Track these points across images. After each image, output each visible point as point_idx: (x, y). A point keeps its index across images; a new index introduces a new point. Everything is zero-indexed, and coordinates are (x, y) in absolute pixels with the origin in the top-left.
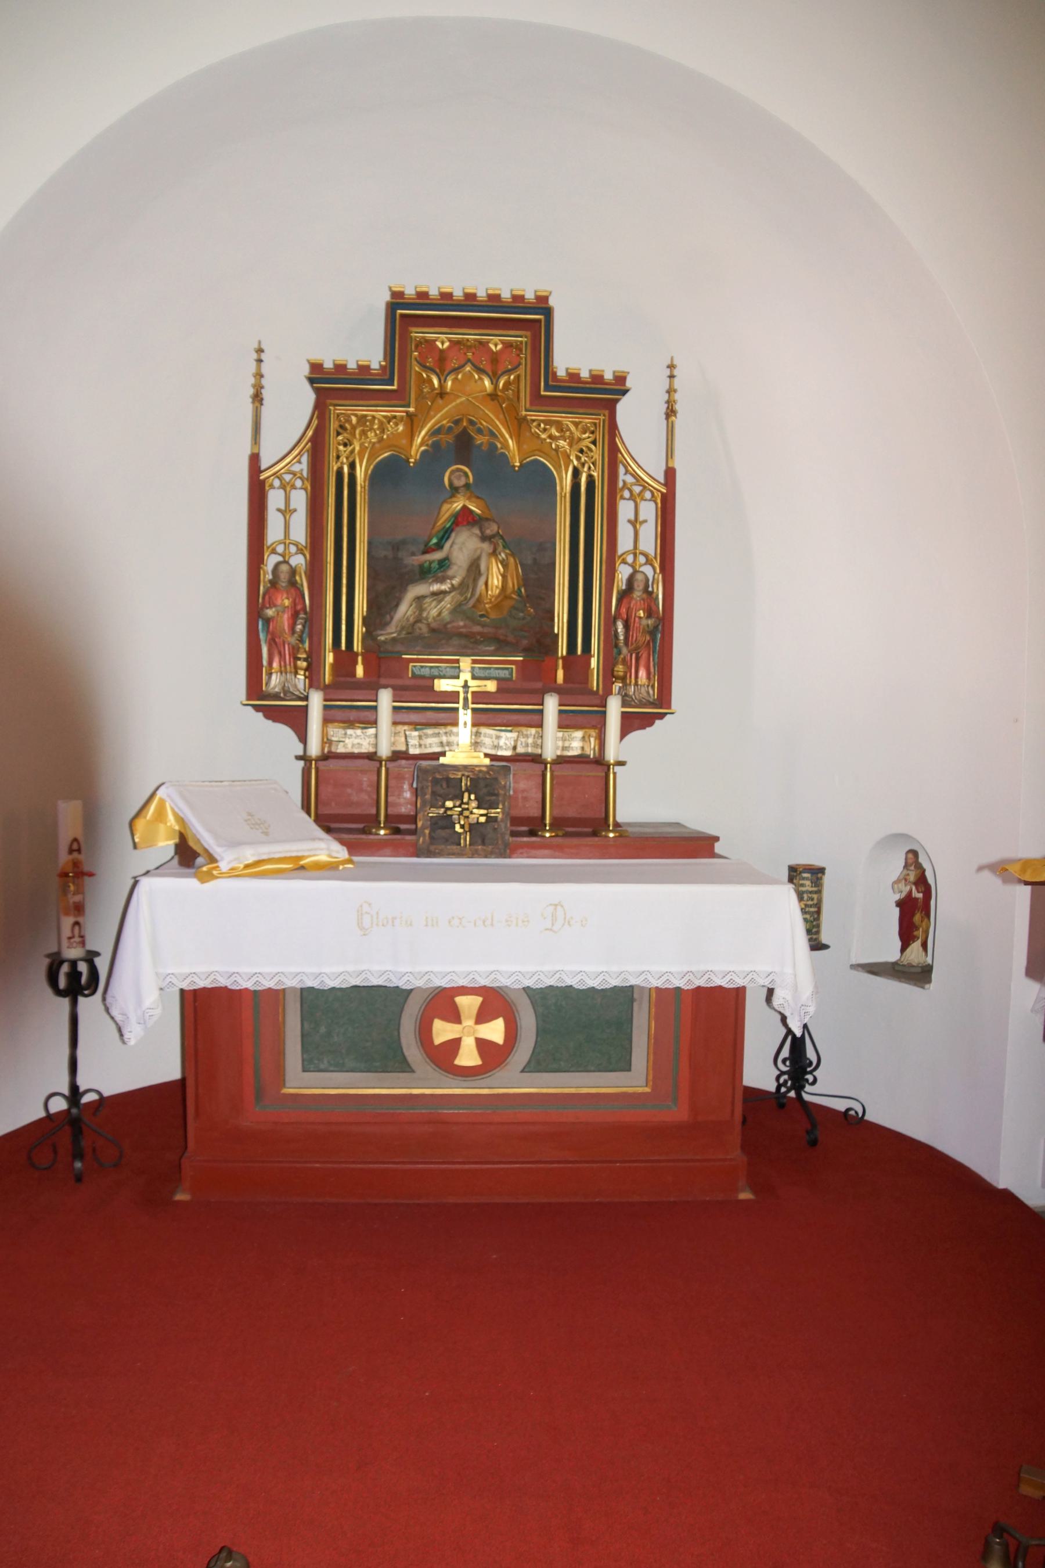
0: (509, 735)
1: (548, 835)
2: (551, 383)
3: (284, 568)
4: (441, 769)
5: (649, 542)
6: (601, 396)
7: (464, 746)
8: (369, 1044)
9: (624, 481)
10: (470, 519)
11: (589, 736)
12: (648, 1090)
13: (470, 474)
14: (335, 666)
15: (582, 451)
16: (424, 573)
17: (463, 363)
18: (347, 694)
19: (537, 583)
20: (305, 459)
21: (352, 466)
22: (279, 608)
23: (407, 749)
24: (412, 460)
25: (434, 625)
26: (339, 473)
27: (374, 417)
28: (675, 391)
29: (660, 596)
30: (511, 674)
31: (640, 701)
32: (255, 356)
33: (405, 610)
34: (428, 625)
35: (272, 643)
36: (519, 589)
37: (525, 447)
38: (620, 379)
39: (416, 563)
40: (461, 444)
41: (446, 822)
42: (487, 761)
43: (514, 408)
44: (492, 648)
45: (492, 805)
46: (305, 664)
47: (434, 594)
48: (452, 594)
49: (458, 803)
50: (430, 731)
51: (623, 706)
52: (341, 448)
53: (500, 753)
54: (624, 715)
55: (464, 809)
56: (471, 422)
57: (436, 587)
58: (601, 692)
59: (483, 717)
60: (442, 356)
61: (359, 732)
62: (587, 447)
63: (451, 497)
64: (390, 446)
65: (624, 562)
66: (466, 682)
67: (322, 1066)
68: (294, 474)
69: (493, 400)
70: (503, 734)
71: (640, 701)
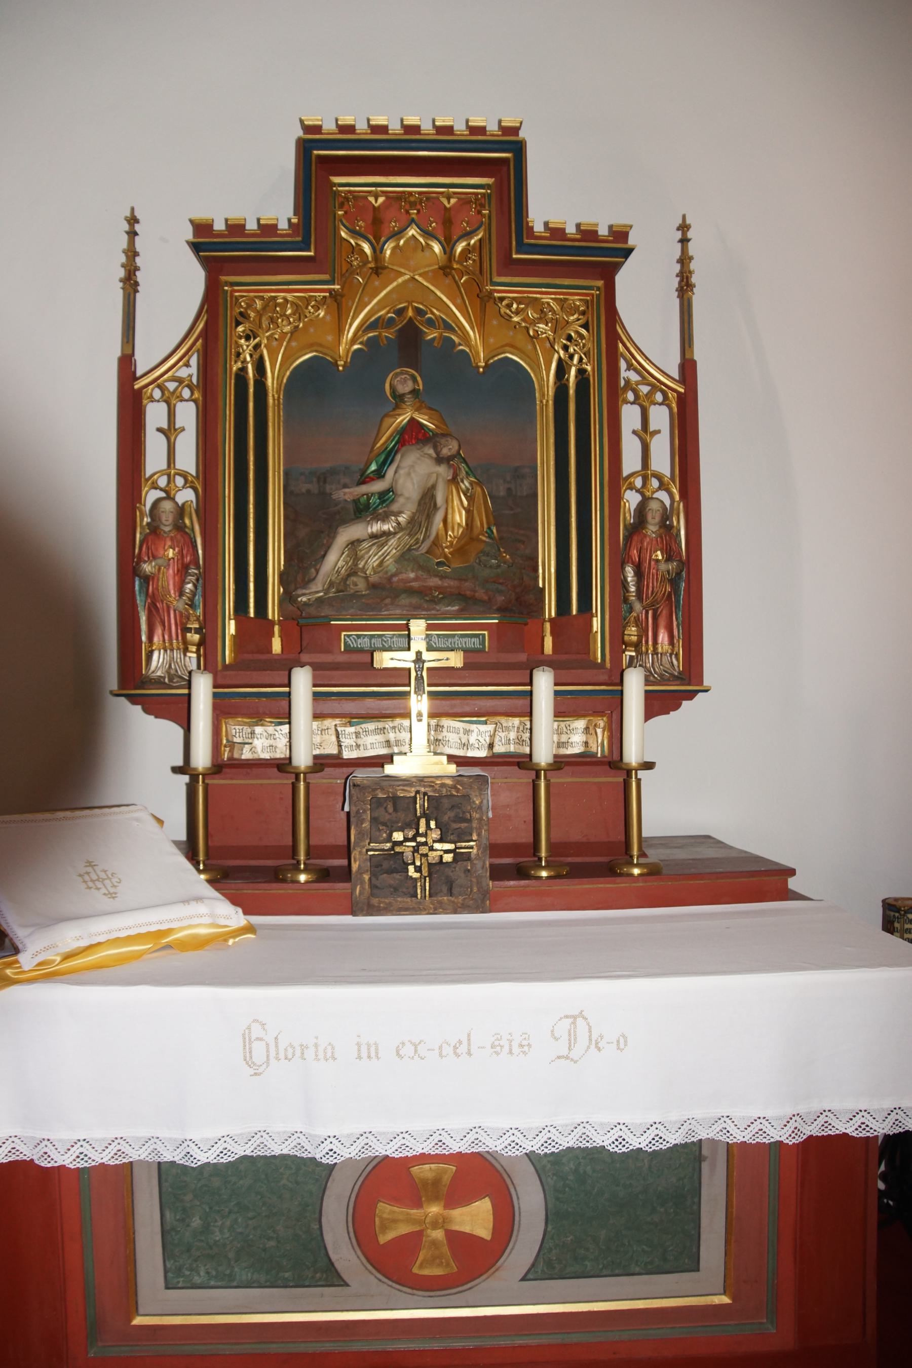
0: (483, 728)
1: (544, 874)
2: (526, 241)
3: (167, 506)
4: (384, 784)
5: (662, 460)
6: (597, 257)
7: (419, 749)
8: (273, 1243)
10: (420, 436)
12: (725, 1300)
13: (419, 379)
14: (238, 639)
15: (569, 338)
16: (362, 510)
18: (256, 677)
19: (511, 517)
20: (194, 361)
22: (160, 561)
23: (340, 752)
25: (374, 579)
27: (285, 299)
28: (691, 258)
29: (683, 532)
31: (661, 675)
32: (126, 227)
33: (334, 560)
34: (366, 578)
35: (153, 611)
36: (489, 528)
37: (492, 340)
38: (620, 234)
39: (349, 498)
40: (407, 340)
41: (394, 862)
42: (452, 769)
44: (456, 608)
45: (463, 836)
46: (197, 637)
47: (373, 536)
49: (411, 834)
50: (371, 726)
51: (646, 685)
52: (243, 341)
53: (470, 754)
54: (649, 696)
55: (420, 844)
56: (419, 312)
57: (376, 527)
58: (608, 665)
59: (445, 705)
61: (271, 729)
62: (577, 332)
63: (394, 409)
64: (312, 345)
65: (631, 487)
66: (419, 654)
67: (197, 1280)
68: (180, 381)
70: (473, 727)
71: (661, 675)
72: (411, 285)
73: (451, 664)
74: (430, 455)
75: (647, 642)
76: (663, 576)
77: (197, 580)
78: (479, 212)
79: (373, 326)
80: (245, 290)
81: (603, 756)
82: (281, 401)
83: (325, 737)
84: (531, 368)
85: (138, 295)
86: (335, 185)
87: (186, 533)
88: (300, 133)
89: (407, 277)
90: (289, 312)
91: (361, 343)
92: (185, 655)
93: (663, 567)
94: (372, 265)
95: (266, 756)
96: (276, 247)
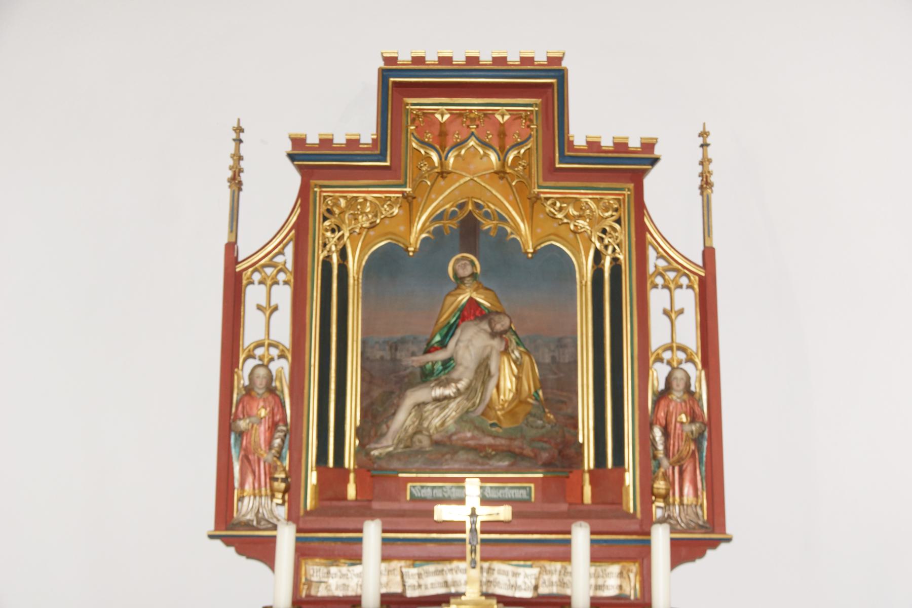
0: (529, 571)
2: (567, 153)
6: (627, 166)
9: (656, 266)
10: (477, 313)
11: (629, 571)
13: (477, 263)
15: (604, 231)
16: (426, 376)
17: (467, 136)
19: (557, 385)
21: (343, 254)
22: (253, 419)
24: (411, 249)
25: (436, 437)
26: (327, 264)
27: (365, 200)
28: (710, 161)
30: (529, 494)
31: (687, 524)
32: (234, 136)
33: (403, 418)
34: (430, 436)
35: (246, 459)
37: (539, 231)
38: (648, 146)
39: (416, 364)
40: (467, 230)
43: (524, 185)
44: (506, 463)
47: (437, 400)
48: (458, 400)
50: (432, 568)
51: (672, 532)
52: (329, 234)
53: (518, 594)
54: (674, 543)
56: (478, 206)
57: (438, 392)
58: (639, 515)
60: (443, 133)
61: (344, 569)
62: (611, 227)
63: (456, 289)
64: (387, 234)
66: (473, 510)
69: (502, 178)
72: (471, 183)
73: (501, 518)
74: (485, 331)
75: (674, 494)
76: (687, 436)
77: (285, 436)
78: (529, 127)
79: (440, 217)
80: (332, 193)
81: (636, 599)
82: (360, 281)
83: (391, 577)
84: (573, 254)
85: (241, 193)
86: (407, 104)
87: (277, 395)
88: (381, 64)
89: (468, 179)
90: (368, 210)
91: (428, 232)
92: (272, 501)
93: (687, 428)
94: (438, 170)
95: (340, 593)
96: (359, 158)
